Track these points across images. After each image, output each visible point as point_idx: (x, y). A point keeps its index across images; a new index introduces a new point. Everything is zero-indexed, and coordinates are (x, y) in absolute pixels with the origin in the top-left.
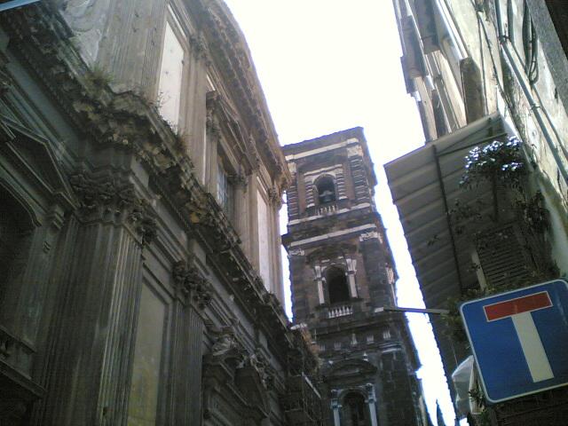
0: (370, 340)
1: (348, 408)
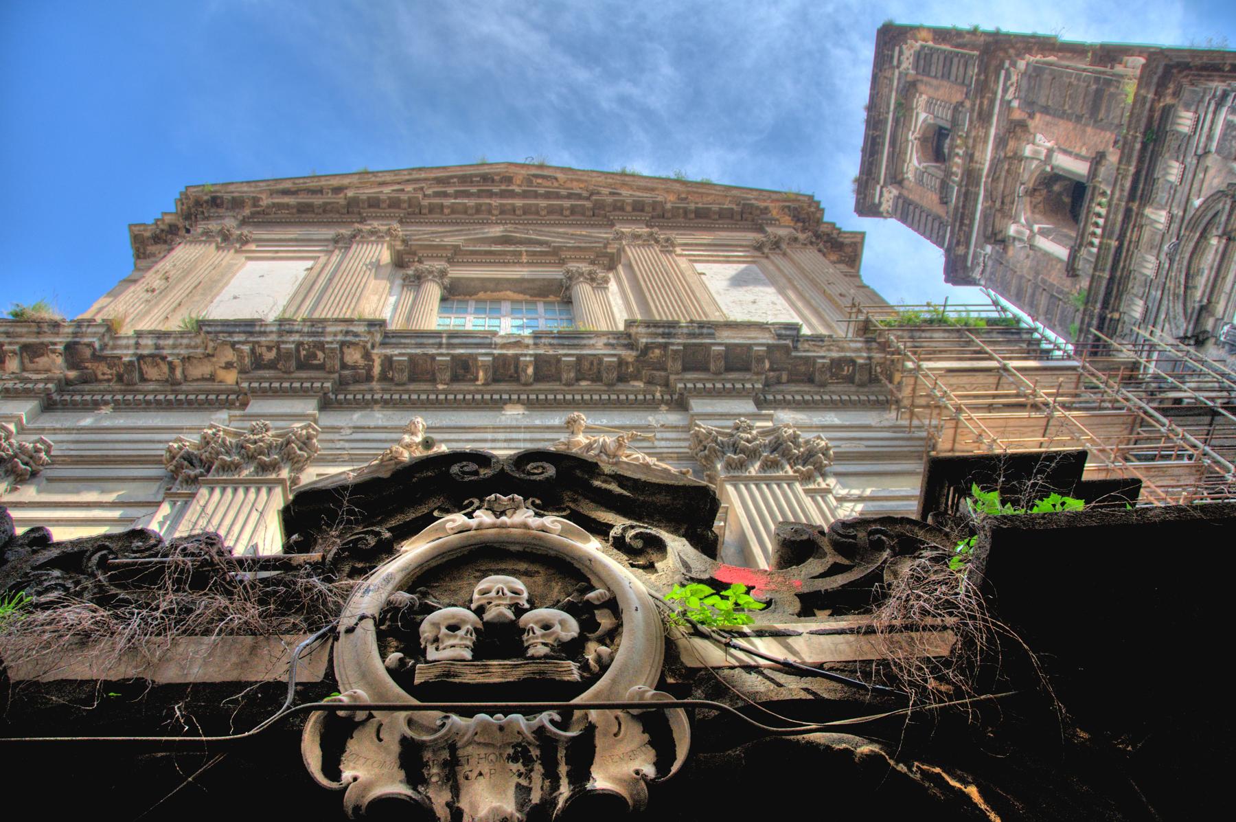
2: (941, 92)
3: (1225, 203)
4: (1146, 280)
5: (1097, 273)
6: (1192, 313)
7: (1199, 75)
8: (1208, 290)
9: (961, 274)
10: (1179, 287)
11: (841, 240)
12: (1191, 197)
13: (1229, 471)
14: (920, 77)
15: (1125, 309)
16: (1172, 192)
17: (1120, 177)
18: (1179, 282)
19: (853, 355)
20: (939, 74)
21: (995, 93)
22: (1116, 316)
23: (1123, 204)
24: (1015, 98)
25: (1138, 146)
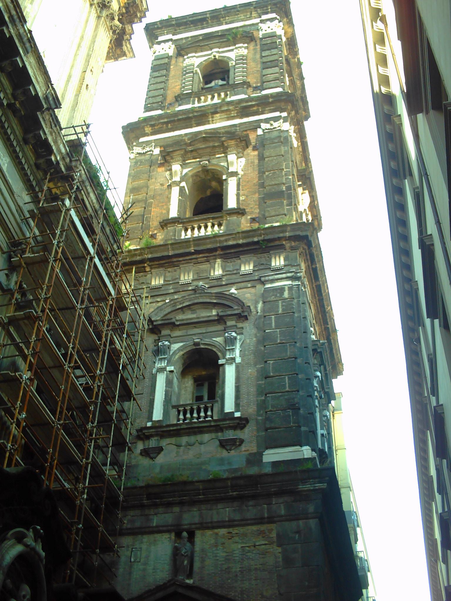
0: (247, 268)
1: (189, 383)
2: (253, 64)
3: (238, 309)
4: (177, 279)
5: (170, 247)
6: (168, 319)
7: (306, 255)
8: (185, 322)
9: (133, 135)
10: (180, 304)
11: (124, 43)
12: (236, 285)
13: (93, 423)
14: (258, 42)
15: (154, 273)
16: (235, 272)
17: (234, 236)
18: (184, 302)
19: (55, 151)
20: (265, 60)
21: (262, 113)
22: (148, 269)
23: (218, 245)
24: (264, 130)
25: (256, 239)
